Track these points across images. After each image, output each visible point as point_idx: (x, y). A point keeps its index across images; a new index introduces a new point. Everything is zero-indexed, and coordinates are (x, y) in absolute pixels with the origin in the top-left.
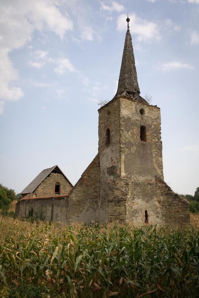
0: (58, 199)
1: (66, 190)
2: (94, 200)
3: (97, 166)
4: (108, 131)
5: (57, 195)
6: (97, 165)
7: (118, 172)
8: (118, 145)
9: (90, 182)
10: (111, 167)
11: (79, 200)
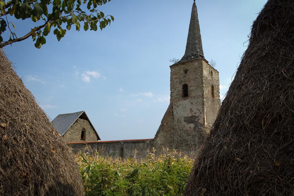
0: (132, 142)
1: (90, 137)
2: (171, 144)
3: (171, 115)
4: (213, 94)
5: (82, 142)
6: (171, 114)
7: (201, 121)
8: (201, 99)
9: (167, 128)
10: (190, 116)
11: (162, 143)
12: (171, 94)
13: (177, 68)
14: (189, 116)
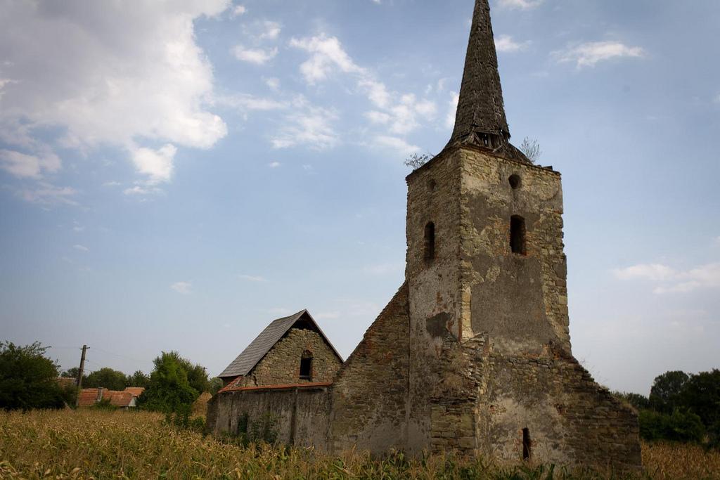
5: (305, 383)
8: (455, 263)
9: (384, 351)
12: (407, 254)
13: (417, 181)
14: (434, 314)
